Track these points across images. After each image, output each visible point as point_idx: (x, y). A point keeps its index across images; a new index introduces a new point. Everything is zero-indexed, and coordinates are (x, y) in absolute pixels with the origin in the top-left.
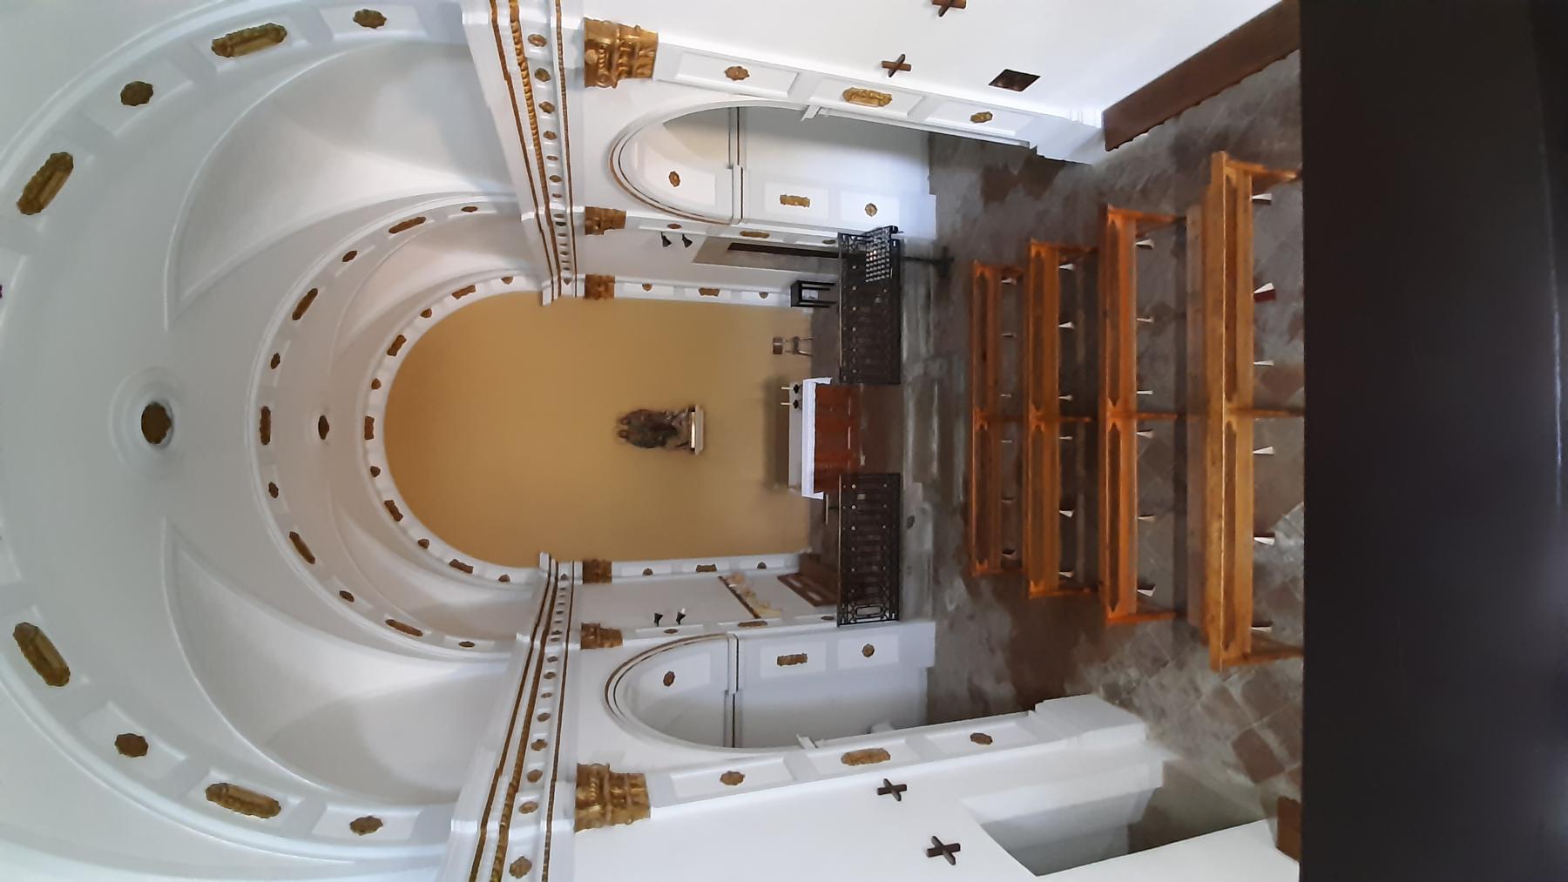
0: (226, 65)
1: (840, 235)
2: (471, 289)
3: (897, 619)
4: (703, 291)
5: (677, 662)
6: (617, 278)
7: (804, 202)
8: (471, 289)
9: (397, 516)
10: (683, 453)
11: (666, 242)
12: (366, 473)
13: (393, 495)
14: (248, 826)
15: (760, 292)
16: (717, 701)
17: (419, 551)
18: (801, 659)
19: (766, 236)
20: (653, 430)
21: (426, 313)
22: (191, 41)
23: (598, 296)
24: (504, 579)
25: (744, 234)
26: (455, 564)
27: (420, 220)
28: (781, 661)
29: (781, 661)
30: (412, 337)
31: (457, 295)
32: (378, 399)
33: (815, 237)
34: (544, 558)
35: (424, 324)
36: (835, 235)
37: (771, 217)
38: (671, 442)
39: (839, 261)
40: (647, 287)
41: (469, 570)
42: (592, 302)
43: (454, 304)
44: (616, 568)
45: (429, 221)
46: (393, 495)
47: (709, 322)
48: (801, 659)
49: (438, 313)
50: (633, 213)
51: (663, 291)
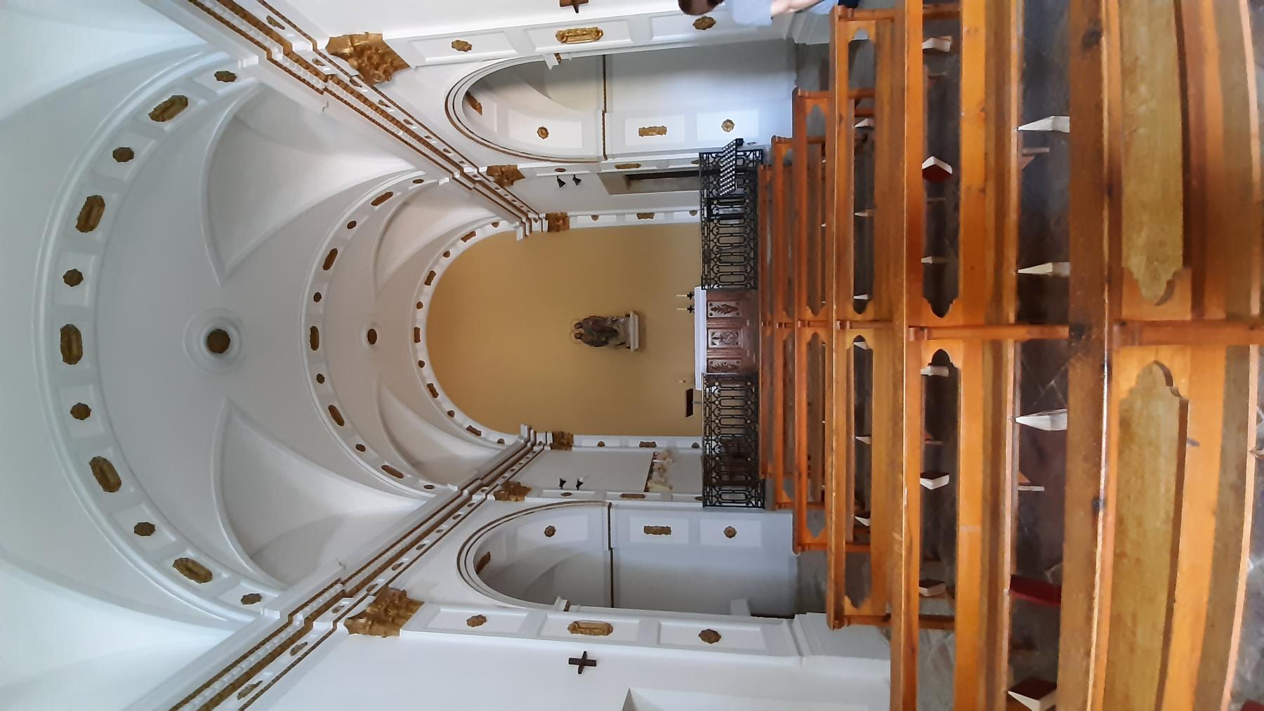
0: (168, 126)
2: (472, 234)
3: (763, 506)
4: (640, 216)
5: (557, 520)
6: (569, 214)
7: (662, 131)
8: (472, 234)
9: (435, 394)
10: (623, 350)
11: (561, 183)
12: (415, 365)
13: (431, 379)
14: (189, 587)
15: (682, 211)
16: (599, 552)
17: (447, 418)
18: (667, 531)
19: (638, 166)
20: (599, 332)
21: (446, 254)
22: (134, 116)
23: (558, 229)
25: (618, 167)
26: (470, 429)
27: (389, 195)
28: (648, 530)
29: (648, 530)
30: (439, 272)
32: (421, 315)
33: (687, 160)
34: (524, 429)
35: (446, 262)
36: (697, 155)
37: (631, 147)
38: (613, 342)
40: (595, 217)
41: (478, 433)
42: (554, 234)
43: (463, 246)
44: (577, 439)
45: (397, 194)
46: (431, 379)
47: (645, 242)
48: (667, 531)
49: (454, 253)
50: (522, 166)
51: (608, 219)
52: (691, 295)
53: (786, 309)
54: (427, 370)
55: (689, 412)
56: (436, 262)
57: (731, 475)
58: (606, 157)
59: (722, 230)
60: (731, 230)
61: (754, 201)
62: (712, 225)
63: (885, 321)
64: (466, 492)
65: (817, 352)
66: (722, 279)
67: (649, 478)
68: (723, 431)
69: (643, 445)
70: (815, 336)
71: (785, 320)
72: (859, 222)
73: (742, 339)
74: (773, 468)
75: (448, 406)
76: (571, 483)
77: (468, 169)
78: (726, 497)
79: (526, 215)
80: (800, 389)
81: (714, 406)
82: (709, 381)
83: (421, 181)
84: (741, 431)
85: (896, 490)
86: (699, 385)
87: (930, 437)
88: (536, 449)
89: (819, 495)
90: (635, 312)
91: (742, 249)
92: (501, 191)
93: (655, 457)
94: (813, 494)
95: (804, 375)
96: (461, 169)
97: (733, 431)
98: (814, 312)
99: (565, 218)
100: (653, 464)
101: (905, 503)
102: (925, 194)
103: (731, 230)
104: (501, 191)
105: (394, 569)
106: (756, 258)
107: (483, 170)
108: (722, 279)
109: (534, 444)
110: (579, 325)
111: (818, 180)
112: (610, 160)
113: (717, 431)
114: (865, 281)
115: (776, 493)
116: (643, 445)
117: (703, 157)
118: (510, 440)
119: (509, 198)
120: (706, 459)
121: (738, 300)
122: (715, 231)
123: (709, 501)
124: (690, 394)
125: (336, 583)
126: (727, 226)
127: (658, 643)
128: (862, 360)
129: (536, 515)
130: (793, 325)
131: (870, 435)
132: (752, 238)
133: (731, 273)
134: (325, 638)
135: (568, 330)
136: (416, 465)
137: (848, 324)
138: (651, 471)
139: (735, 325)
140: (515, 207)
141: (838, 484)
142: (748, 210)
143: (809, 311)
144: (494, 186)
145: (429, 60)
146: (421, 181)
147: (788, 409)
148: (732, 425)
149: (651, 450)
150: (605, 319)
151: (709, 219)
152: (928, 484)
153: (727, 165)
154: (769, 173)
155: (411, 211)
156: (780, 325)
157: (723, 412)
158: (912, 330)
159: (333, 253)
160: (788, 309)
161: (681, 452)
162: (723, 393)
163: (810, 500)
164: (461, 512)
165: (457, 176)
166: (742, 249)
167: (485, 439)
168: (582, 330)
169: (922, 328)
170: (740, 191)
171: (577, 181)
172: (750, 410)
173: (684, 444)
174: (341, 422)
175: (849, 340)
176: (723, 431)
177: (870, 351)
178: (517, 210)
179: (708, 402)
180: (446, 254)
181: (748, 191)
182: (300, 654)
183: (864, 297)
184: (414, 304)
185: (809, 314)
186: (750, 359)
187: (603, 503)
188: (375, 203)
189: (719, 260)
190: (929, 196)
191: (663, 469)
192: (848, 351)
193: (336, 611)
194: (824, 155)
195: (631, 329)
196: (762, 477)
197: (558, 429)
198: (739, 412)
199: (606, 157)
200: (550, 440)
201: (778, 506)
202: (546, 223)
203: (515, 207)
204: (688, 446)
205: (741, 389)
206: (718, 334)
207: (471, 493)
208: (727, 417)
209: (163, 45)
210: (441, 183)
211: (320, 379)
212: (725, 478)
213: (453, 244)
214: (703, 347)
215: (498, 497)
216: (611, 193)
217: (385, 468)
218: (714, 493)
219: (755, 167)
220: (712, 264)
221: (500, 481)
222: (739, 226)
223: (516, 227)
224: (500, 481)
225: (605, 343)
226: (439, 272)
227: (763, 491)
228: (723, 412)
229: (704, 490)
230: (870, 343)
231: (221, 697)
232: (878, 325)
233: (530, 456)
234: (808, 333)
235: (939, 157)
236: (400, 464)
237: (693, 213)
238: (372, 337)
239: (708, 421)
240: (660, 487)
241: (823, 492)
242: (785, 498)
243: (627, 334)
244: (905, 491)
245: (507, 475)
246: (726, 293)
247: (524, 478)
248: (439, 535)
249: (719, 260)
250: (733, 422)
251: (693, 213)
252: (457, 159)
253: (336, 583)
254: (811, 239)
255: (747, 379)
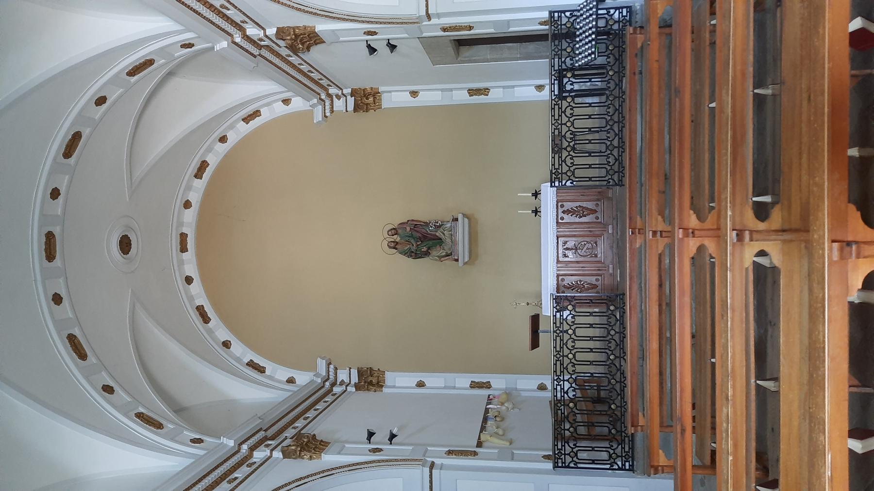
1: (551, 13)
2: (256, 114)
3: (632, 469)
4: (472, 92)
8: (256, 114)
9: (206, 319)
10: (448, 262)
11: (372, 50)
12: (181, 282)
13: (202, 300)
15: (526, 86)
17: (222, 351)
19: (470, 28)
20: (420, 240)
21: (223, 139)
24: (291, 381)
25: (444, 30)
26: (251, 365)
27: (149, 63)
30: (213, 160)
31: (247, 120)
32: (190, 216)
34: (322, 365)
36: (545, 15)
38: (435, 253)
39: (545, 47)
40: (414, 94)
42: (361, 114)
43: (244, 129)
47: (481, 120)
49: (233, 138)
50: (322, 27)
51: (430, 97)
52: (536, 194)
53: (661, 213)
54: (196, 288)
55: (535, 343)
56: (210, 150)
57: (590, 425)
58: (429, 17)
59: (577, 111)
60: (589, 111)
61: (621, 73)
62: (565, 104)
63: (799, 230)
64: (245, 447)
65: (705, 271)
66: (578, 173)
67: (483, 428)
68: (579, 368)
69: (474, 385)
70: (701, 249)
71: (661, 226)
72: (759, 100)
73: (603, 249)
74: (646, 419)
75: (223, 334)
76: (381, 436)
77: (252, 31)
78: (583, 455)
79: (326, 90)
80: (682, 317)
81: (566, 337)
82: (560, 302)
83: (190, 46)
84: (601, 369)
85: (814, 454)
86: (547, 309)
87: (856, 382)
88: (337, 390)
89: (708, 460)
90: (464, 215)
91: (604, 135)
92: (294, 59)
93: (489, 400)
94: (699, 454)
95: (687, 299)
96: (242, 30)
97: (592, 369)
98: (699, 218)
99: (375, 94)
100: (487, 411)
101: (828, 473)
102: (848, 66)
103: (589, 111)
104: (294, 59)
105: (236, 478)
106: (621, 147)
107: (271, 31)
108: (578, 173)
109: (333, 384)
110: (394, 231)
111: (707, 45)
112: (434, 21)
113: (570, 369)
114: (768, 178)
115: (650, 454)
116: (474, 385)
117: (554, 17)
118: (303, 378)
119: (305, 68)
120: (556, 404)
121: (601, 196)
122: (568, 112)
123: (561, 461)
124: (535, 320)
125: (260, 430)
126: (582, 105)
127: (512, 459)
128: (764, 279)
129: (338, 477)
130: (671, 234)
131: (776, 379)
132: (616, 120)
133: (588, 166)
134: (266, 461)
135: (379, 239)
136: (179, 410)
137: (747, 235)
138: (485, 420)
139: (594, 233)
140: (300, 71)
141: (735, 445)
142: (612, 85)
143: (693, 217)
144: (284, 52)
145: (341, 39)
146: (190, 46)
147: (666, 341)
148: (589, 361)
149: (485, 392)
150: (427, 224)
151: (561, 97)
152: (857, 446)
153: (586, 27)
154: (640, 39)
155: (175, 82)
156: (655, 233)
157: (578, 344)
158: (835, 245)
159: (77, 137)
160: (666, 210)
161: (524, 394)
162: (579, 320)
163: (697, 462)
164: (239, 474)
165: (238, 40)
166: (604, 135)
167: (270, 378)
168: (397, 238)
169: (849, 244)
170: (601, 60)
171: (392, 47)
172: (614, 341)
173: (527, 384)
174: (83, 356)
175: (749, 255)
176: (579, 368)
177: (775, 270)
178: (316, 84)
179: (559, 332)
180: (223, 139)
181: (611, 60)
182: (254, 467)
183: (767, 199)
184: (179, 203)
185: (693, 221)
186: (613, 275)
187: (421, 462)
188: (132, 73)
189: (573, 149)
190: (852, 68)
191: (500, 417)
192: (747, 269)
193: (316, 410)
194: (713, 13)
195: (459, 236)
196: (631, 430)
197: (365, 365)
198: (598, 344)
199: (429, 17)
200: (355, 379)
201: (653, 469)
202: (351, 101)
203: (300, 71)
204: (533, 386)
205: (600, 314)
206: (570, 244)
207: (252, 449)
208: (583, 350)
209: (151, 28)
210: (218, 47)
211: (57, 299)
212: (582, 430)
213: (232, 127)
214: (549, 256)
215: (286, 454)
216: (434, 63)
217: (139, 416)
218: (568, 450)
219: (622, 30)
220: (565, 154)
221: (290, 432)
222: (600, 105)
223: (313, 106)
224: (290, 432)
225: (427, 254)
226: (213, 160)
227: (632, 448)
228: (578, 344)
229: (555, 445)
230: (776, 257)
231: (217, 483)
232: (787, 236)
233: (329, 399)
234: (692, 245)
235: (867, 17)
236: (159, 409)
237: (540, 88)
238: (125, 245)
239: (559, 356)
240: (496, 441)
241: (713, 453)
242: (662, 459)
243: (454, 243)
244: (829, 458)
245: (299, 424)
246: (584, 188)
247: (320, 428)
248: (317, 412)
249: (573, 149)
250: (591, 357)
251: (540, 88)
252: (238, 18)
253: (260, 430)
254: (696, 122)
255: (612, 301)
